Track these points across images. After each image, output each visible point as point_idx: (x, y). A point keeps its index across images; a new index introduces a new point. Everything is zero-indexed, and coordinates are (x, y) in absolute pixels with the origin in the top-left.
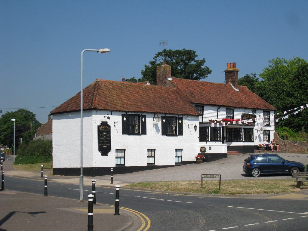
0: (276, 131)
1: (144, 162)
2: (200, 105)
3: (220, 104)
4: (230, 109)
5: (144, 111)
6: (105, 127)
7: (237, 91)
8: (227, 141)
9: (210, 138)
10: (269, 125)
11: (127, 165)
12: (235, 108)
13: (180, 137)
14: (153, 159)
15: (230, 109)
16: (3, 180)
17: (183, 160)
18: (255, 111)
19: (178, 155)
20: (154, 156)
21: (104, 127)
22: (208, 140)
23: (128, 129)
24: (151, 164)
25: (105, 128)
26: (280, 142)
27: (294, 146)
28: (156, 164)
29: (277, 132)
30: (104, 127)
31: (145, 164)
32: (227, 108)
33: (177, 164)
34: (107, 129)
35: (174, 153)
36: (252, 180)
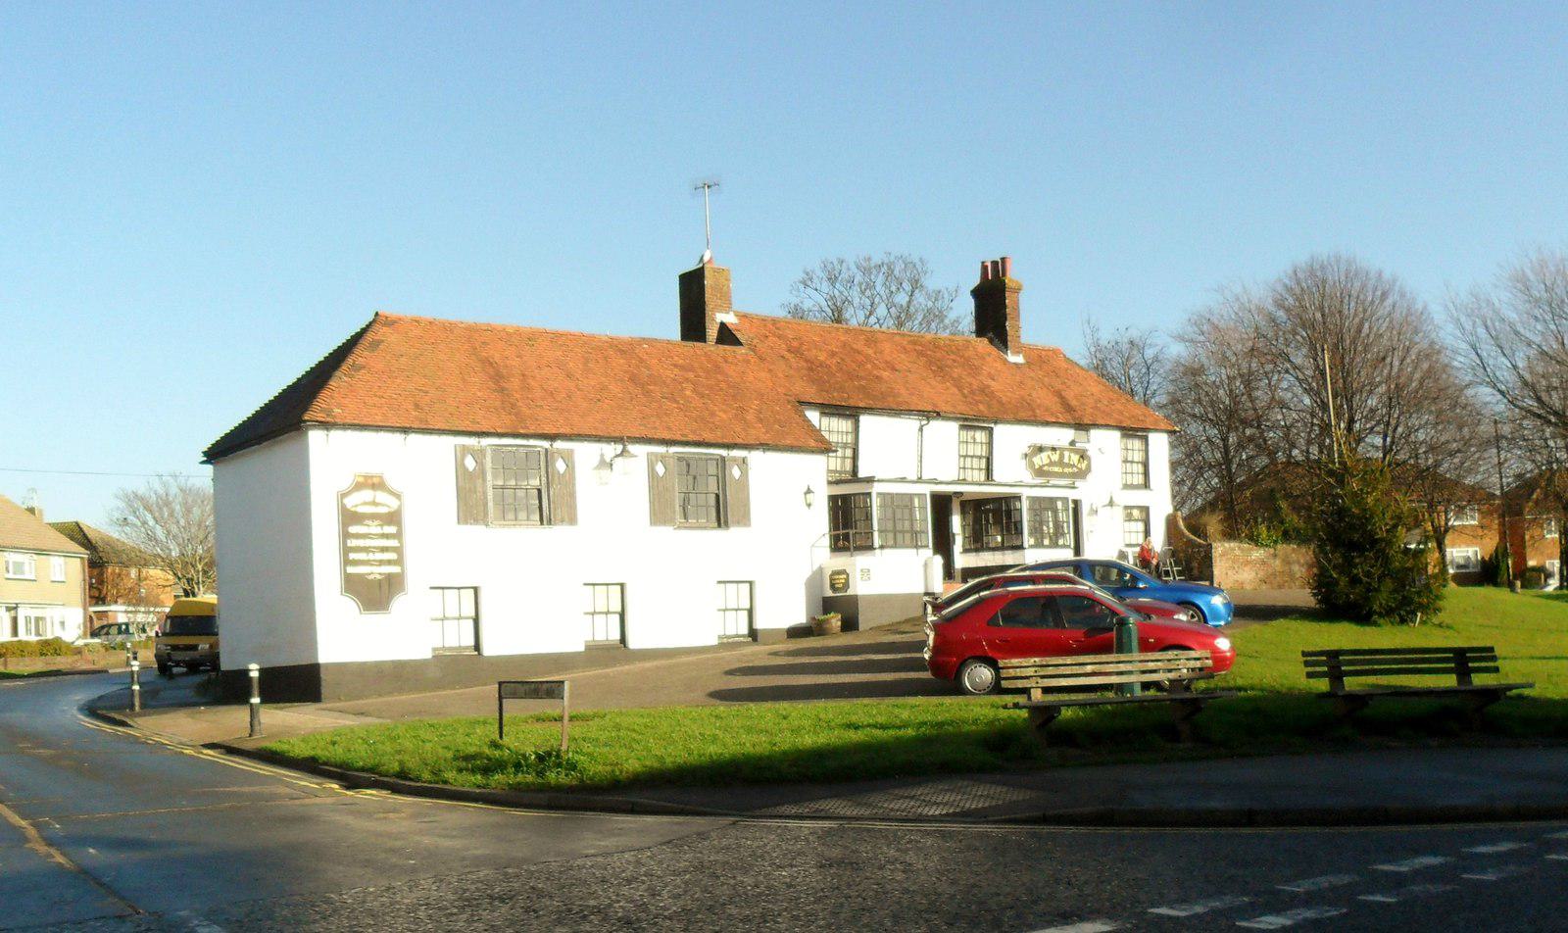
31: (423, 653)
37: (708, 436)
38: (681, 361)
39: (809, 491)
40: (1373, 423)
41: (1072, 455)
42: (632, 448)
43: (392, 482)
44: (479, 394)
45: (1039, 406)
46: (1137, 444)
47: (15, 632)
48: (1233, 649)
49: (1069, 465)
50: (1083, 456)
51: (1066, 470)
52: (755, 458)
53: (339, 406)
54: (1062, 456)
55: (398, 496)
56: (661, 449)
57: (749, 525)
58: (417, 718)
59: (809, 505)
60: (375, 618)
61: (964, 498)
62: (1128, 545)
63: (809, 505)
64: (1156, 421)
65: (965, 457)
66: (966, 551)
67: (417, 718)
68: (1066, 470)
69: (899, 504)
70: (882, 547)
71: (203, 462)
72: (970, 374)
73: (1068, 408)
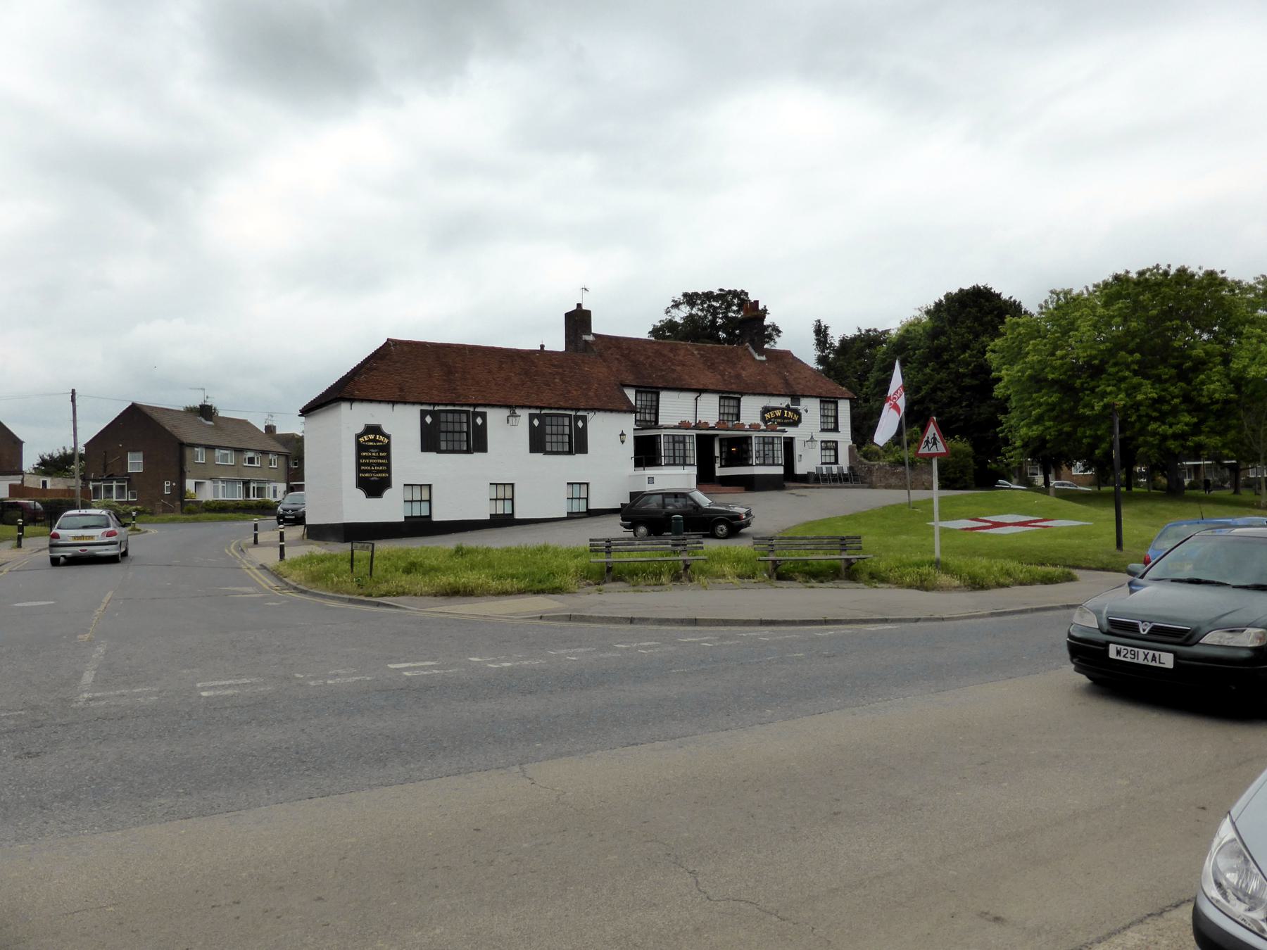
0: (853, 443)
1: (483, 512)
2: (832, 400)
3: (701, 387)
4: (731, 396)
5: (479, 402)
6: (375, 437)
7: (761, 361)
8: (723, 464)
9: (663, 455)
10: (836, 429)
11: (435, 518)
12: (743, 394)
13: (579, 457)
14: (508, 504)
15: (731, 396)
16: (283, 543)
17: (591, 507)
18: (796, 398)
19: (501, 495)
20: (661, 496)
21: (372, 437)
22: (751, 463)
23: (431, 441)
24: (421, 517)
25: (374, 440)
26: (860, 466)
27: (894, 474)
28: (517, 516)
29: (855, 445)
30: (372, 437)
31: (400, 518)
32: (637, 389)
33: (572, 516)
34: (381, 441)
35: (564, 492)
36: (411, 568)
37: (562, 404)
38: (556, 363)
39: (622, 434)
40: (302, 624)
41: (790, 413)
42: (518, 412)
43: (386, 430)
44: (437, 382)
45: (770, 385)
46: (832, 406)
47: (248, 495)
48: (1139, 367)
49: (787, 418)
50: (797, 412)
51: (786, 421)
52: (590, 415)
53: (358, 390)
54: (783, 413)
55: (388, 437)
56: (537, 412)
57: (587, 453)
58: (1152, 333)
59: (623, 442)
60: (374, 501)
61: (720, 437)
62: (822, 464)
63: (623, 442)
64: (843, 393)
65: (724, 414)
66: (722, 466)
67: (1152, 333)
68: (786, 421)
69: (677, 441)
70: (666, 465)
71: (300, 415)
72: (1235, 307)
73: (787, 383)
